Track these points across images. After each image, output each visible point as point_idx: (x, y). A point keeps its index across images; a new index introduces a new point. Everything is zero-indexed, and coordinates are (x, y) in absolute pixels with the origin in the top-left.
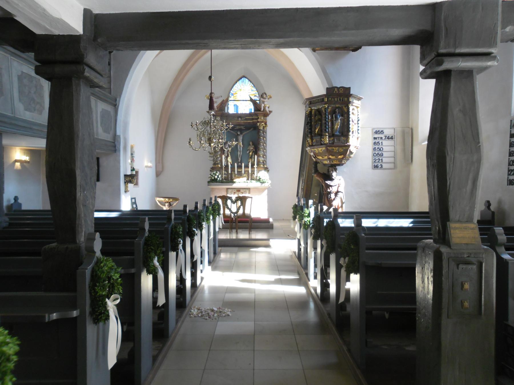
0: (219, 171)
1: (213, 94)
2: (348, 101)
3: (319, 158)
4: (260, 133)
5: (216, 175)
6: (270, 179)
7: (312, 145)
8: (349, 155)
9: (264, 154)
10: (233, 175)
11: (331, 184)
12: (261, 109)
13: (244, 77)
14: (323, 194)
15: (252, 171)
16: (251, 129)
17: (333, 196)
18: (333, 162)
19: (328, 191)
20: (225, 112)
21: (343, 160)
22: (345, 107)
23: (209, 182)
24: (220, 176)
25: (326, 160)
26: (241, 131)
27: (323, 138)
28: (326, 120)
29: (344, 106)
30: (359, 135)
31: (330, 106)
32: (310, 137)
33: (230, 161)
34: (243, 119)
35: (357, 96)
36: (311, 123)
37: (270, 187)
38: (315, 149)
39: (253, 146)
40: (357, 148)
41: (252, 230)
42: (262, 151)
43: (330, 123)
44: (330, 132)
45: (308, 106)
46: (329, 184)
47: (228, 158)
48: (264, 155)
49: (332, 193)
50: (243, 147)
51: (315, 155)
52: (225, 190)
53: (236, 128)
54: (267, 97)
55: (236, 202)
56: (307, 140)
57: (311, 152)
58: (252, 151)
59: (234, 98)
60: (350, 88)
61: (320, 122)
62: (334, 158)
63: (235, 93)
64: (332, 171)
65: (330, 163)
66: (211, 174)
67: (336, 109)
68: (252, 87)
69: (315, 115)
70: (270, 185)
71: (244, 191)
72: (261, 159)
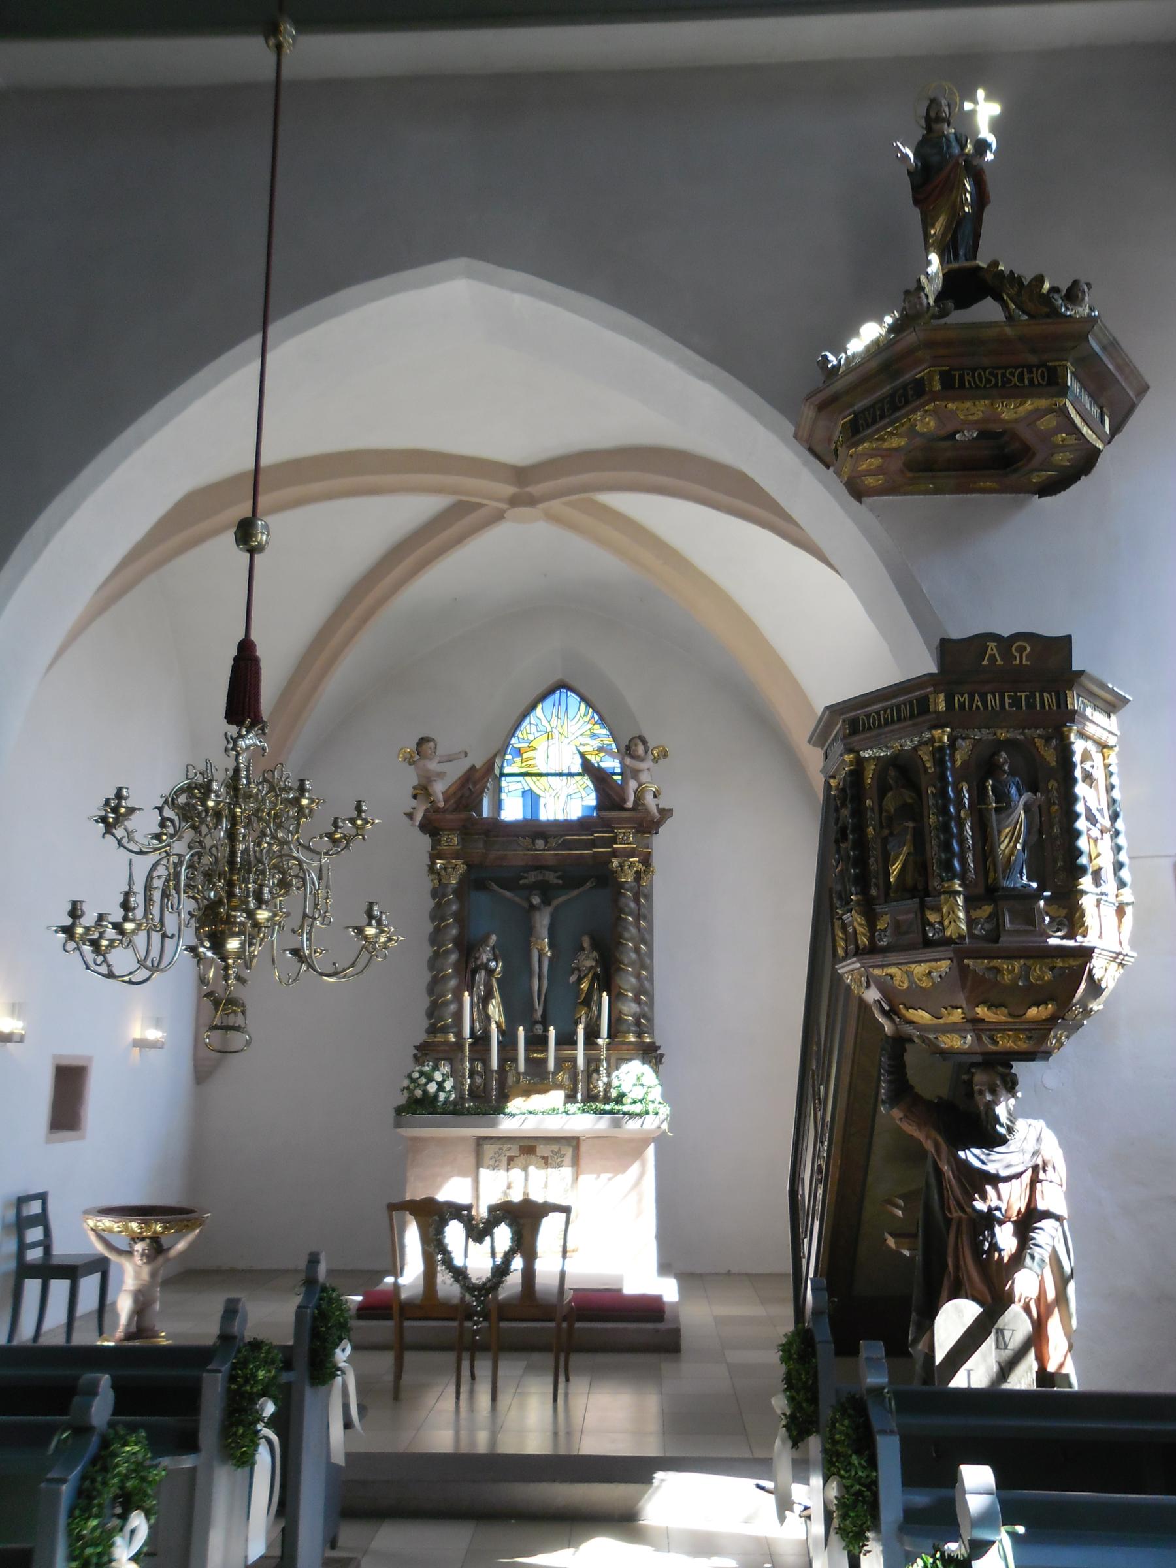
0: (451, 1061)
1: (431, 744)
2: (1059, 706)
3: (915, 1019)
4: (623, 900)
5: (430, 1079)
6: (667, 1097)
7: (873, 949)
8: (1084, 1003)
9: (642, 985)
10: (511, 1079)
11: (991, 1168)
12: (625, 801)
13: (563, 685)
14: (948, 1221)
15: (589, 1061)
16: (589, 884)
17: (1006, 1239)
18: (996, 1043)
19: (973, 1208)
20: (480, 812)
21: (1052, 1034)
22: (1048, 740)
23: (399, 1111)
24: (448, 1085)
25: (952, 1028)
26: (547, 892)
27: (938, 909)
28: (944, 811)
29: (1040, 736)
30: (1127, 895)
31: (964, 739)
32: (858, 903)
33: (497, 1019)
34: (553, 842)
35: (1103, 686)
36: (860, 829)
37: (664, 1132)
38: (893, 970)
39: (595, 954)
40: (1121, 964)
41: (575, 1359)
42: (632, 974)
43: (971, 828)
44: (972, 874)
45: (839, 747)
46: (976, 1163)
47: (491, 1006)
48: (644, 992)
49: (1001, 1223)
50: (551, 960)
51: (890, 1003)
52: (472, 1145)
53: (526, 878)
54: (650, 752)
55: (491, 1234)
56: (838, 923)
57: (868, 986)
58: (590, 976)
59: (523, 765)
60: (1068, 640)
61: (910, 824)
62: (1003, 1018)
63: (526, 745)
64: (993, 1091)
65: (978, 1049)
66: (409, 1076)
67: (996, 753)
68: (596, 723)
69: (883, 789)
70: (665, 1126)
71: (552, 1151)
72: (629, 1009)
